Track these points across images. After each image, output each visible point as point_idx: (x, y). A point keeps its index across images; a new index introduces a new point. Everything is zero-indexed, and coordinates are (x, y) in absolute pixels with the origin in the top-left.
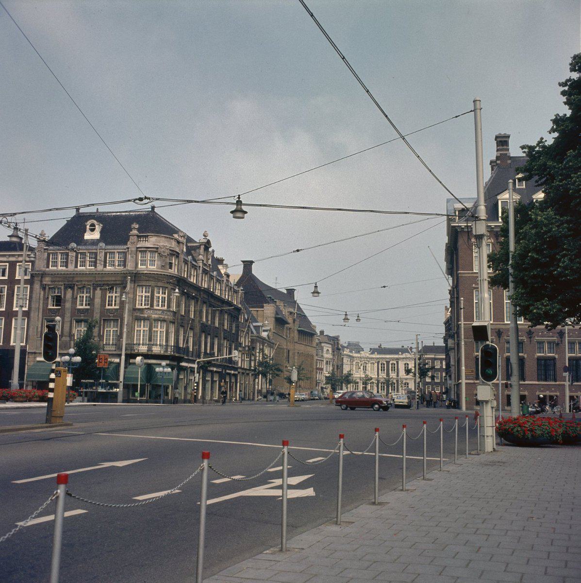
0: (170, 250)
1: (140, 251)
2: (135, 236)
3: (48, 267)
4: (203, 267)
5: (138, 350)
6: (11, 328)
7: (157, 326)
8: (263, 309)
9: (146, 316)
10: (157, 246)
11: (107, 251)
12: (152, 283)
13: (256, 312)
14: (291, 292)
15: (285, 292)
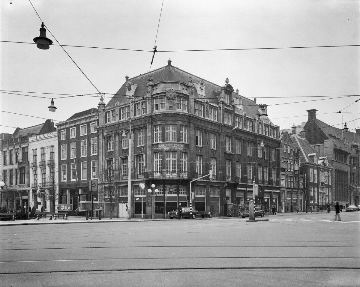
0: (177, 93)
1: (154, 98)
2: (150, 87)
3: (106, 122)
4: (223, 107)
5: (183, 176)
6: (91, 168)
7: (182, 157)
8: (323, 144)
9: (160, 149)
10: (165, 91)
11: (135, 103)
12: (163, 123)
13: (323, 146)
14: (140, 74)
15: (355, 132)
